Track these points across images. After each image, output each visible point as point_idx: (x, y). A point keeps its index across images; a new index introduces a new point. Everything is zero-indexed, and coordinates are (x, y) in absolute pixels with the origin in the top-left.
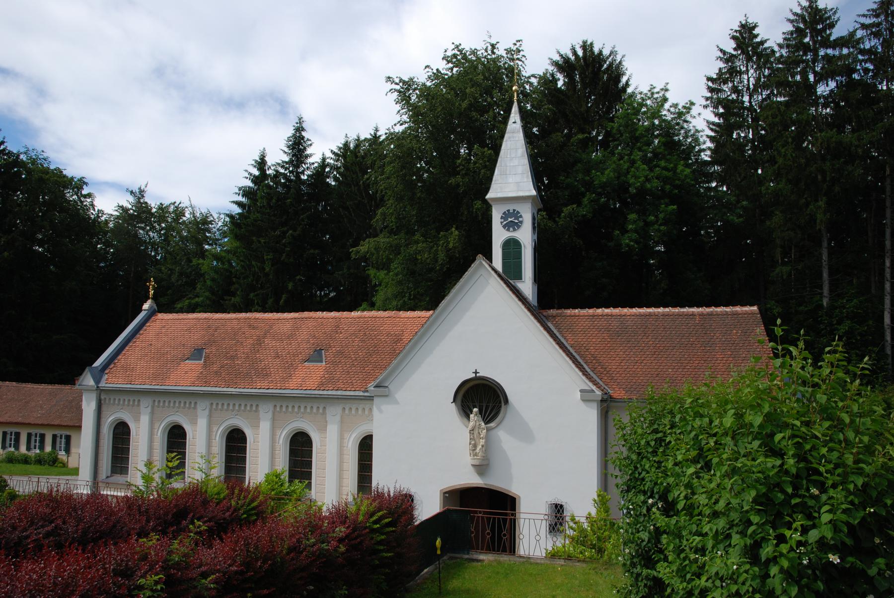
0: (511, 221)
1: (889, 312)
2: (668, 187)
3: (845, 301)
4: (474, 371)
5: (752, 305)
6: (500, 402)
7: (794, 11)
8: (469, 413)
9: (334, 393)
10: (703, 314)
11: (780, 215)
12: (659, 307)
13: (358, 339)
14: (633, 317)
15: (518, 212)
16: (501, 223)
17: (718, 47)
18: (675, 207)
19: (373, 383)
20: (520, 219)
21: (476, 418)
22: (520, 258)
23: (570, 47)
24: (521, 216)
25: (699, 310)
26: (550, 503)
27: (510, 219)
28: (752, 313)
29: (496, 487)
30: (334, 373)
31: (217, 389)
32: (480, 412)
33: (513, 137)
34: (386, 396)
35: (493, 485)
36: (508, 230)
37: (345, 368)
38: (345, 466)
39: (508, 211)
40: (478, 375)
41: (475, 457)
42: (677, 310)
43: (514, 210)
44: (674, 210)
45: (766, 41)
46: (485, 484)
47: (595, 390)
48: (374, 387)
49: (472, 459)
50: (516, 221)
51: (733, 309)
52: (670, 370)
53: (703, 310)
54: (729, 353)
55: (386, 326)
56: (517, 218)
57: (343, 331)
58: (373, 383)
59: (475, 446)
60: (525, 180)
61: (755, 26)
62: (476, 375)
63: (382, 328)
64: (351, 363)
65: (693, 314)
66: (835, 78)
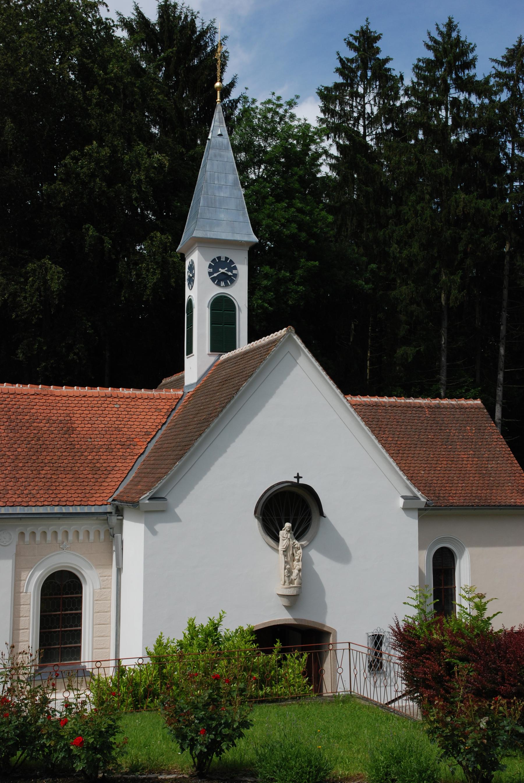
0: (223, 273)
1: (501, 405)
2: (304, 234)
3: (463, 391)
5: (475, 398)
6: (310, 514)
7: (432, 35)
8: (279, 529)
10: (431, 406)
11: (412, 285)
12: (140, 388)
15: (232, 262)
16: (210, 274)
17: (338, 54)
18: (317, 263)
19: (148, 494)
20: (234, 272)
21: (289, 535)
22: (234, 323)
24: (235, 268)
25: (425, 401)
26: (371, 634)
27: (222, 271)
28: (477, 408)
29: (308, 621)
32: (293, 528)
33: (221, 156)
34: (163, 511)
35: (305, 620)
36: (218, 284)
38: (23, 622)
39: (219, 258)
41: (291, 585)
42: (402, 400)
43: (227, 259)
44: (315, 266)
46: (295, 620)
47: (420, 497)
48: (149, 499)
49: (287, 588)
50: (230, 274)
51: (459, 402)
53: (429, 402)
54: (471, 452)
56: (231, 269)
58: (148, 494)
59: (290, 572)
60: (241, 219)
61: (378, 38)
63: (33, 411)
65: (421, 407)
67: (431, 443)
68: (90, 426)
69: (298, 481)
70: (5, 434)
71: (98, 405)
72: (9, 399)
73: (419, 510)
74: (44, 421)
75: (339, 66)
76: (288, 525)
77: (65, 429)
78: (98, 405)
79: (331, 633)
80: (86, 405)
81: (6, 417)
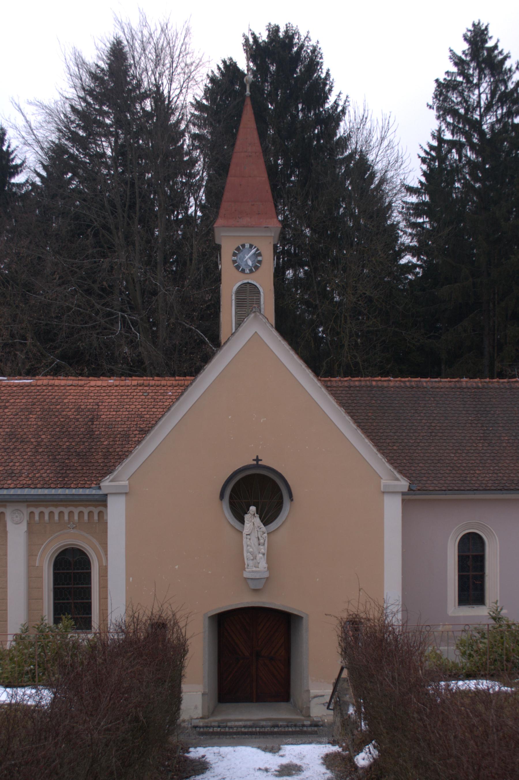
4: (255, 458)
6: (281, 498)
9: (19, 492)
13: (34, 416)
14: (97, 388)
23: (471, 23)
30: (11, 464)
31: (46, 492)
37: (26, 457)
40: (260, 463)
45: (218, 66)
52: (453, 455)
55: (71, 397)
57: (7, 404)
62: (257, 463)
63: (66, 401)
64: (33, 450)
66: (114, 125)
67: (470, 425)
68: (114, 413)
69: (257, 463)
70: (35, 422)
71: (128, 394)
72: (47, 391)
73: (403, 494)
74: (73, 410)
75: (476, 24)
76: (253, 509)
77: (90, 417)
78: (128, 394)
79: (302, 618)
80: (116, 394)
81: (41, 407)
